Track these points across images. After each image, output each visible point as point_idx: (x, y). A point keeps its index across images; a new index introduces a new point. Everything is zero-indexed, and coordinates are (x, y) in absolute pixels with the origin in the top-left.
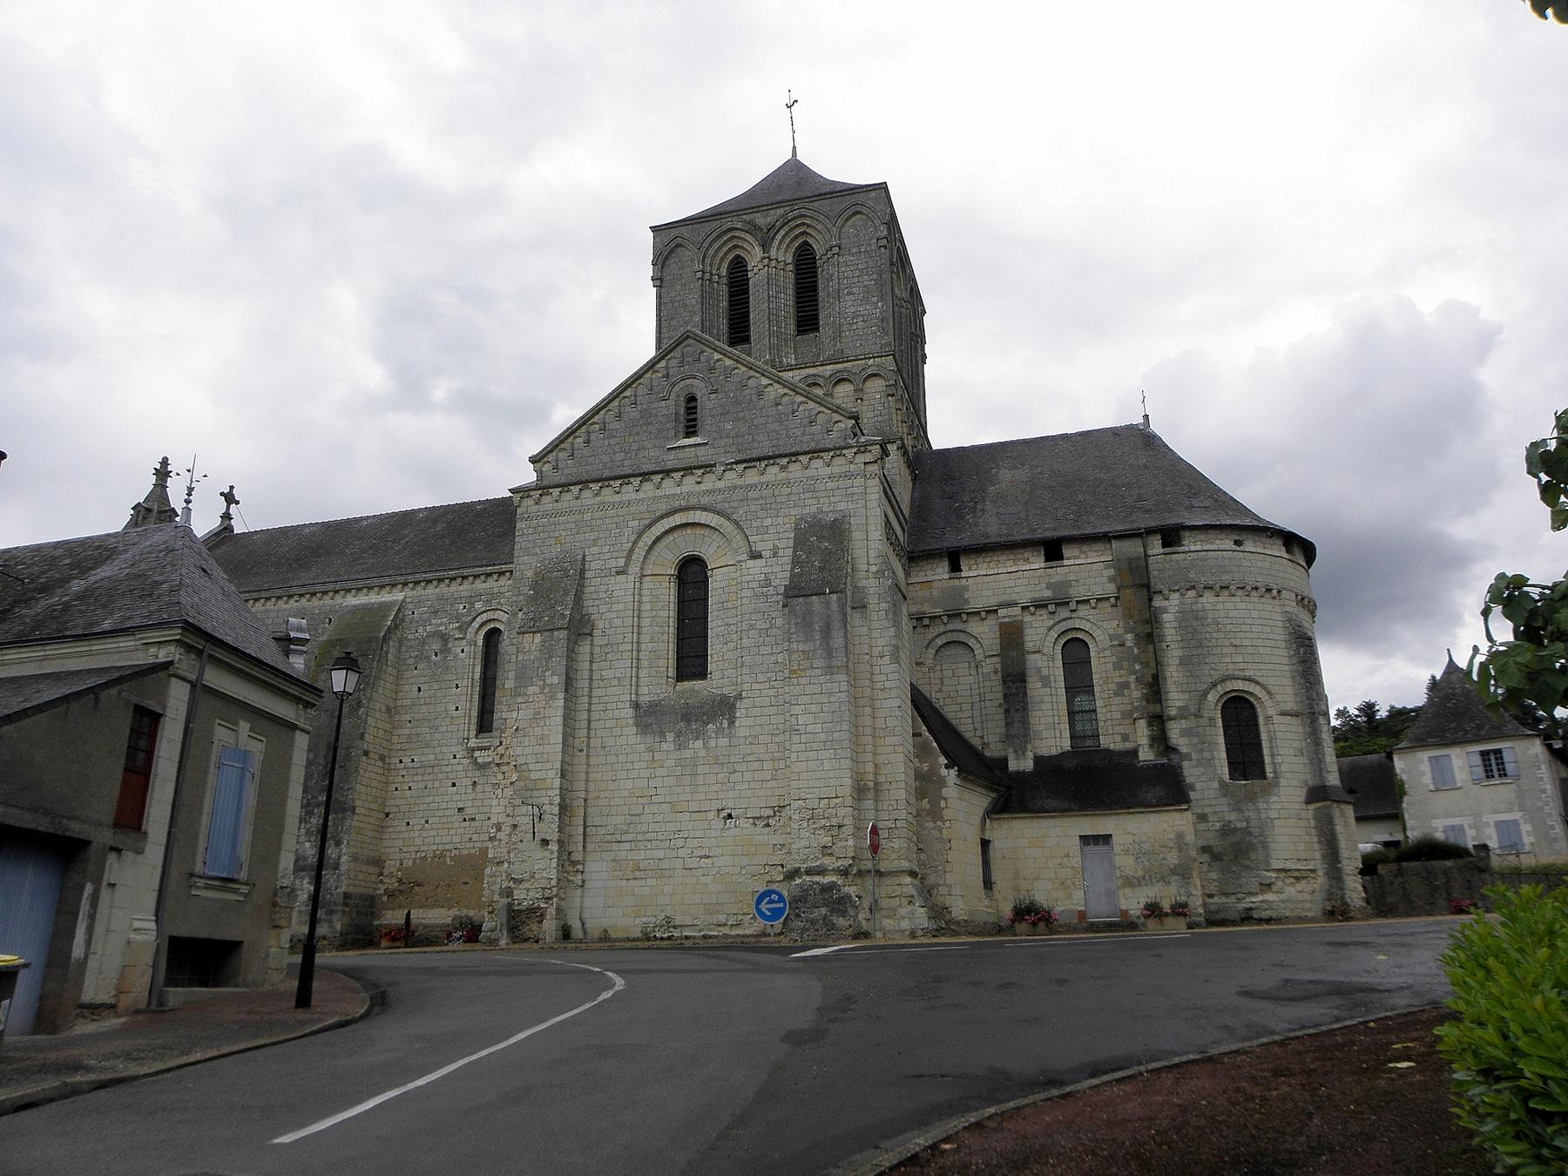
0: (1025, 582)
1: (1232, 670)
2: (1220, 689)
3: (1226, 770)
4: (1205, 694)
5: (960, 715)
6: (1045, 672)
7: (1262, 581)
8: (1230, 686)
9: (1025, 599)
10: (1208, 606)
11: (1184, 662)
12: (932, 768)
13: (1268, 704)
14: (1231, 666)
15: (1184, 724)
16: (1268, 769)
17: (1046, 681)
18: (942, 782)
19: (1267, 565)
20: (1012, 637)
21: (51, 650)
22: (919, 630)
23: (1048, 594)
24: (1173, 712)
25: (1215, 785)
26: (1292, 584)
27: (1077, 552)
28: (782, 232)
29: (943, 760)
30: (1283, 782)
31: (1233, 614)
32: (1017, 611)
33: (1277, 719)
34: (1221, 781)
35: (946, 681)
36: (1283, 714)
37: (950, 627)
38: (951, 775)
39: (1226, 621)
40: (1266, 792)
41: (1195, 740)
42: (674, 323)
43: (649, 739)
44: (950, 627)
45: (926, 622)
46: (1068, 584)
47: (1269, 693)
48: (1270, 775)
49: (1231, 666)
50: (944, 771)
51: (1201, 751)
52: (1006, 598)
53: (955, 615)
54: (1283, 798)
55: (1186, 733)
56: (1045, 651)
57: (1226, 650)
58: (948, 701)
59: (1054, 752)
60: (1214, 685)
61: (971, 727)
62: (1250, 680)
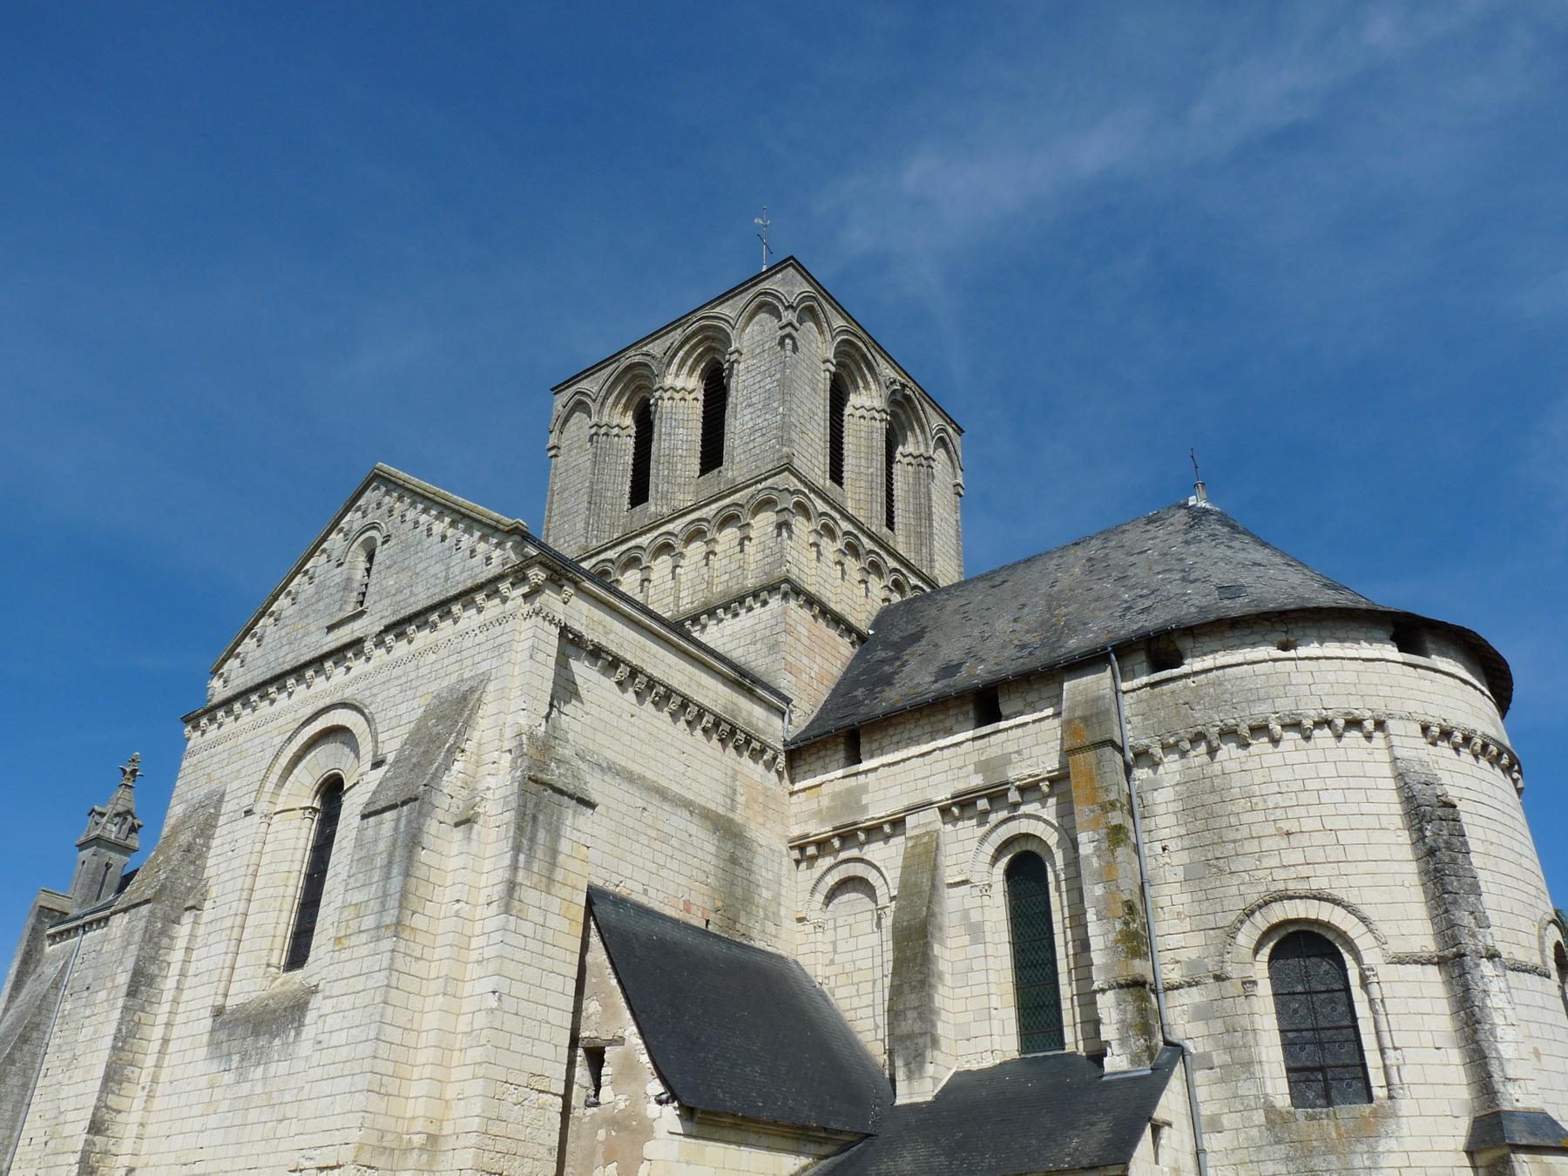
0: (945, 765)
1: (1283, 880)
2: (1262, 922)
3: (1282, 1086)
4: (1232, 932)
5: (856, 1002)
6: (975, 916)
7: (1338, 706)
8: (1279, 912)
9: (943, 795)
10: (1231, 766)
11: (1192, 876)
12: (634, 1101)
13: (1363, 941)
14: (1280, 874)
15: (1193, 996)
16: (1376, 1078)
17: (976, 932)
18: (645, 1131)
19: (1349, 677)
20: (924, 860)
21: (1365, 1046)
22: (803, 865)
23: (976, 781)
24: (1172, 974)
25: (1259, 1117)
26: (1411, 706)
27: (1019, 705)
28: (681, 354)
29: (656, 1087)
30: (1405, 1106)
31: (1281, 775)
32: (933, 815)
33: (1385, 972)
34: (1270, 1109)
35: (841, 947)
36: (1401, 960)
37: (844, 855)
38: (669, 1116)
39: (1266, 789)
40: (1368, 1132)
41: (1218, 1026)
42: (566, 494)
43: (214, 1066)
44: (844, 855)
45: (811, 850)
46: (1005, 760)
47: (1363, 920)
48: (1379, 1092)
49: (1280, 874)
50: (653, 1109)
51: (1230, 1048)
52: (917, 799)
53: (847, 836)
54: (1409, 1144)
55: (1201, 1014)
56: (975, 879)
57: (1268, 844)
58: (842, 979)
59: (989, 1062)
60: (1250, 913)
61: (869, 1024)
62: (1319, 897)
